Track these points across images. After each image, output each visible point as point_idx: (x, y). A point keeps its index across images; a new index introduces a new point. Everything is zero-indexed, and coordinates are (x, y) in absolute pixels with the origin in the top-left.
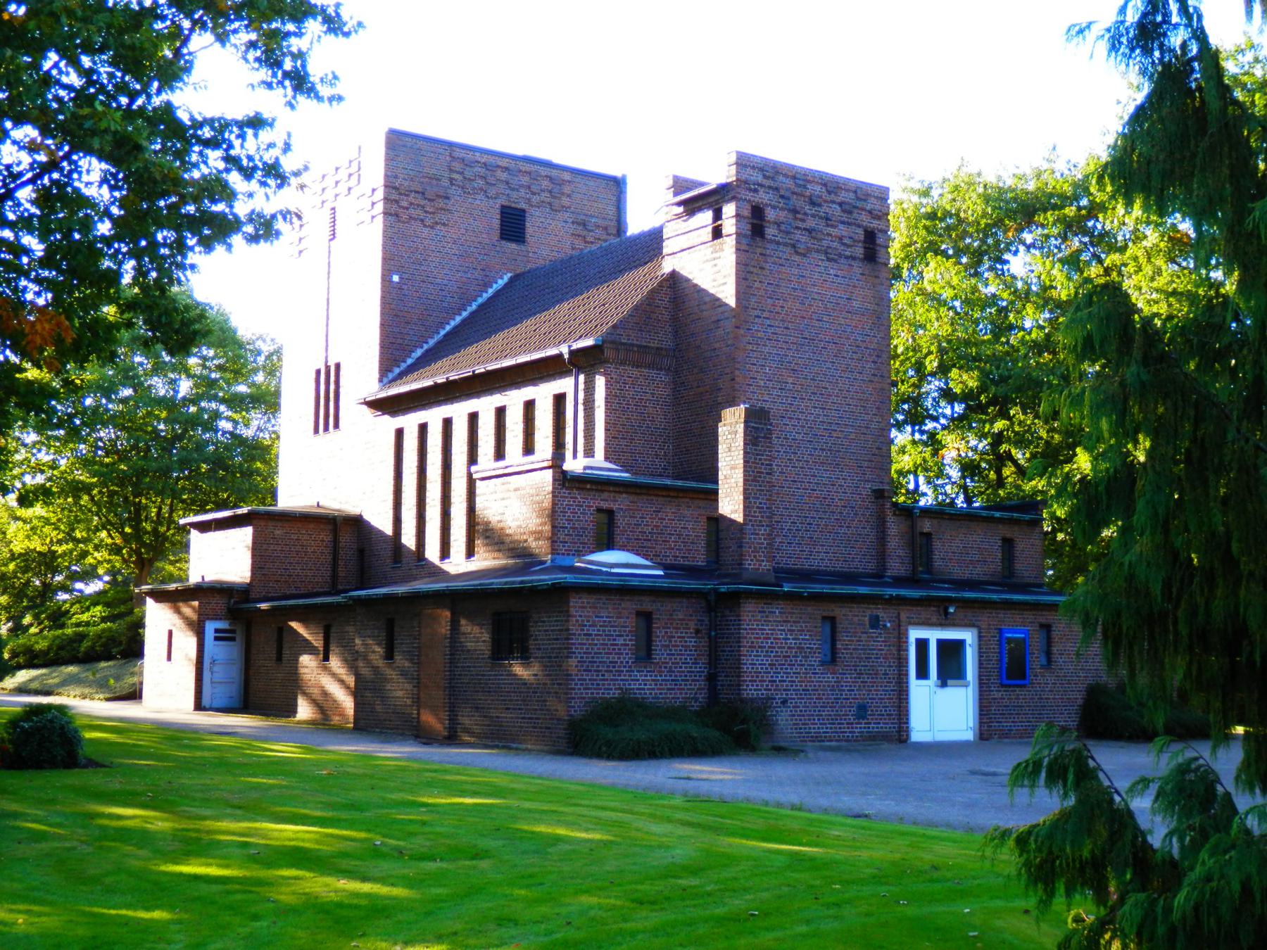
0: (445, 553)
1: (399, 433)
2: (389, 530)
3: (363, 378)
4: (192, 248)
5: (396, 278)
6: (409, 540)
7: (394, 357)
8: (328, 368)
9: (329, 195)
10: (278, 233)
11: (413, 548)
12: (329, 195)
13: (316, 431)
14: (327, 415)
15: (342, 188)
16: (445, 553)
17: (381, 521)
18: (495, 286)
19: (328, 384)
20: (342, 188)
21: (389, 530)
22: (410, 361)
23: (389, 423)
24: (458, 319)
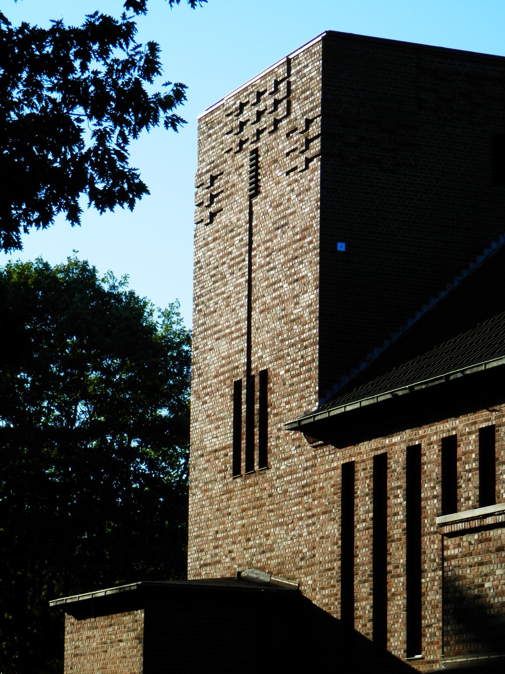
0: (414, 643)
1: (348, 471)
2: (335, 610)
3: (295, 397)
4: (21, 76)
5: (341, 247)
6: (363, 625)
7: (333, 379)
8: (250, 378)
9: (249, 132)
10: (194, 280)
11: (337, 616)
12: (249, 132)
13: (236, 471)
14: (250, 450)
15: (267, 121)
16: (414, 643)
17: (324, 595)
18: (486, 252)
19: (252, 394)
20: (267, 121)
21: (335, 610)
22: (364, 366)
23: (334, 458)
24: (434, 302)
